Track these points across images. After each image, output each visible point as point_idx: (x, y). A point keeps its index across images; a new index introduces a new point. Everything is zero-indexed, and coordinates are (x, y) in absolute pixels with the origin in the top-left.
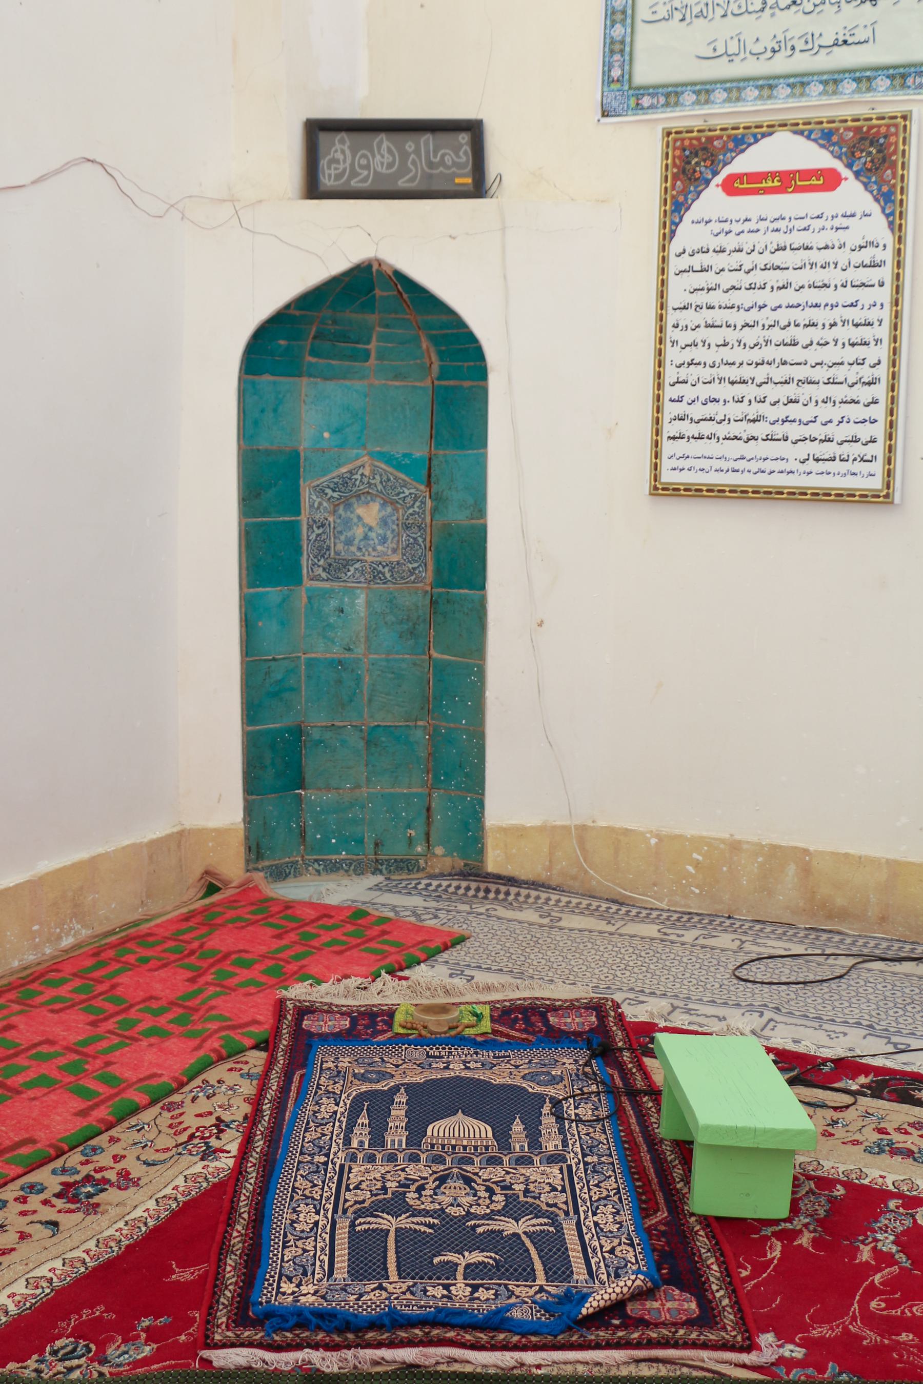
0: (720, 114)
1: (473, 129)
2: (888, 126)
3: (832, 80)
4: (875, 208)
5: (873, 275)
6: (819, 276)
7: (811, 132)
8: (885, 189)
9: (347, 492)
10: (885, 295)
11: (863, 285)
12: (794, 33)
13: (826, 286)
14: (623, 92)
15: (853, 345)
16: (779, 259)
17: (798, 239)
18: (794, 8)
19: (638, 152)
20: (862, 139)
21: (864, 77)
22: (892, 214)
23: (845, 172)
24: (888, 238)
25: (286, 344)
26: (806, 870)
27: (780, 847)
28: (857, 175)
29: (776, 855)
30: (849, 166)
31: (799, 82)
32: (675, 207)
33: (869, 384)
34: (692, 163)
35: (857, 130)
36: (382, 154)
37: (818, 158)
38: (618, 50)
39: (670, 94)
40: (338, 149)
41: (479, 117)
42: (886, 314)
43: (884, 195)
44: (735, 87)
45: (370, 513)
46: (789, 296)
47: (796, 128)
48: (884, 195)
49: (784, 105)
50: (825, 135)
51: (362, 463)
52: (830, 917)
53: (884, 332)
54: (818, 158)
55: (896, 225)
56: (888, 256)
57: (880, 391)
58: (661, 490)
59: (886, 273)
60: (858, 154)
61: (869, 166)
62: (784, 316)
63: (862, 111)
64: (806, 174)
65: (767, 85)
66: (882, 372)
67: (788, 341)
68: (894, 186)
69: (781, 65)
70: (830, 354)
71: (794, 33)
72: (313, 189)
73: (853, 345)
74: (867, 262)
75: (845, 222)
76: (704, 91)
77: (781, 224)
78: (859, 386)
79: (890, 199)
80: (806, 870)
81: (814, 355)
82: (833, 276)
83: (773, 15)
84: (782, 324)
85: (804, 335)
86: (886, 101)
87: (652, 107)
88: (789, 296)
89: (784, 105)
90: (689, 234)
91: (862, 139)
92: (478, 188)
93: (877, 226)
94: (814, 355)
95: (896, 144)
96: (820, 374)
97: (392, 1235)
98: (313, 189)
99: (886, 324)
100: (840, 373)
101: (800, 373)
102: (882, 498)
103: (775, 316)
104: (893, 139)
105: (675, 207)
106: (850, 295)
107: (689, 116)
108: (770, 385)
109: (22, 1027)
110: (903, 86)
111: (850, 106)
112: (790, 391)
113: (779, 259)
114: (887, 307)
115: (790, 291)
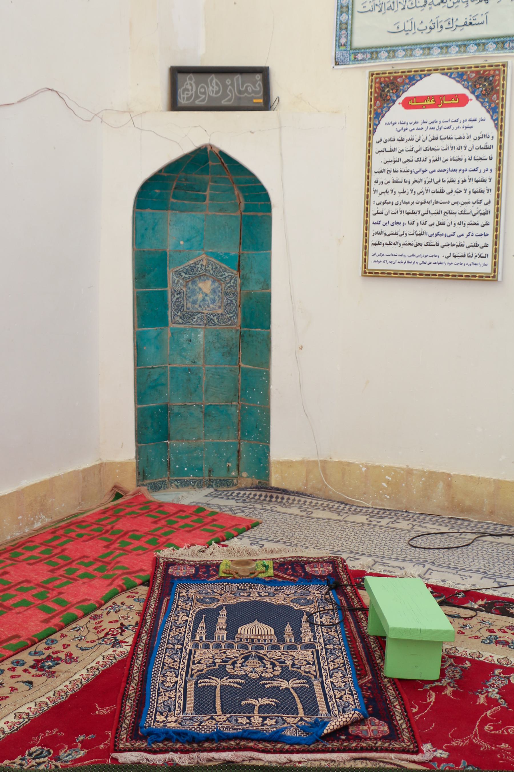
0: (401, 63)
1: (263, 72)
2: (495, 70)
3: (463, 45)
4: (488, 116)
5: (486, 153)
6: (456, 154)
7: (451, 73)
8: (493, 105)
9: (193, 275)
10: (493, 164)
11: (481, 159)
12: (442, 18)
13: (460, 159)
14: (347, 51)
15: (475, 192)
16: (434, 144)
17: (445, 133)
18: (442, 5)
19: (355, 85)
20: (480, 77)
21: (481, 43)
22: (497, 119)
23: (471, 96)
24: (494, 133)
25: (159, 192)
26: (449, 486)
27: (435, 472)
28: (477, 97)
29: (432, 477)
30: (473, 93)
31: (445, 46)
32: (376, 115)
33: (484, 214)
34: (386, 91)
35: (477, 72)
36: (213, 86)
37: (456, 88)
38: (344, 28)
39: (373, 53)
40: (188, 83)
41: (267, 65)
42: (493, 175)
43: (492, 109)
44: (409, 49)
45: (206, 286)
46: (439, 165)
47: (443, 72)
48: (492, 109)
49: (436, 59)
50: (460, 75)
51: (202, 258)
52: (462, 511)
53: (492, 185)
54: (456, 88)
55: (499, 126)
56: (494, 143)
57: (490, 218)
58: (368, 273)
59: (493, 152)
60: (478, 86)
61: (484, 92)
62: (437, 176)
63: (480, 62)
64: (449, 97)
65: (427, 47)
66: (491, 207)
67: (439, 190)
68: (498, 104)
69: (435, 36)
70: (462, 197)
71: (442, 18)
72: (174, 105)
73: (475, 192)
74: (483, 146)
75: (471, 124)
76: (392, 50)
77: (435, 125)
78: (478, 215)
79: (496, 111)
80: (449, 486)
81: (453, 198)
82: (464, 154)
83: (430, 8)
84: (436, 181)
85: (448, 187)
86: (493, 56)
87: (363, 60)
88: (439, 165)
89: (436, 59)
90: (383, 130)
91: (480, 77)
92: (266, 105)
93: (488, 126)
94: (453, 198)
95: (499, 80)
96: (457, 209)
97: (218, 689)
98: (174, 105)
99: (494, 181)
100: (468, 208)
101: (445, 208)
102: (491, 278)
103: (432, 176)
104: (497, 78)
105: (376, 115)
106: (473, 164)
107: (384, 65)
108: (429, 215)
109: (12, 573)
110: (503, 48)
111: (473, 59)
112: (440, 218)
113: (434, 144)
114: (494, 171)
115: (440, 162)
